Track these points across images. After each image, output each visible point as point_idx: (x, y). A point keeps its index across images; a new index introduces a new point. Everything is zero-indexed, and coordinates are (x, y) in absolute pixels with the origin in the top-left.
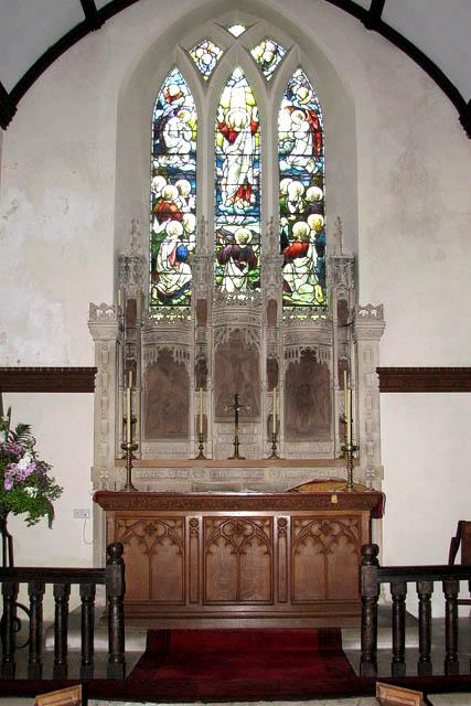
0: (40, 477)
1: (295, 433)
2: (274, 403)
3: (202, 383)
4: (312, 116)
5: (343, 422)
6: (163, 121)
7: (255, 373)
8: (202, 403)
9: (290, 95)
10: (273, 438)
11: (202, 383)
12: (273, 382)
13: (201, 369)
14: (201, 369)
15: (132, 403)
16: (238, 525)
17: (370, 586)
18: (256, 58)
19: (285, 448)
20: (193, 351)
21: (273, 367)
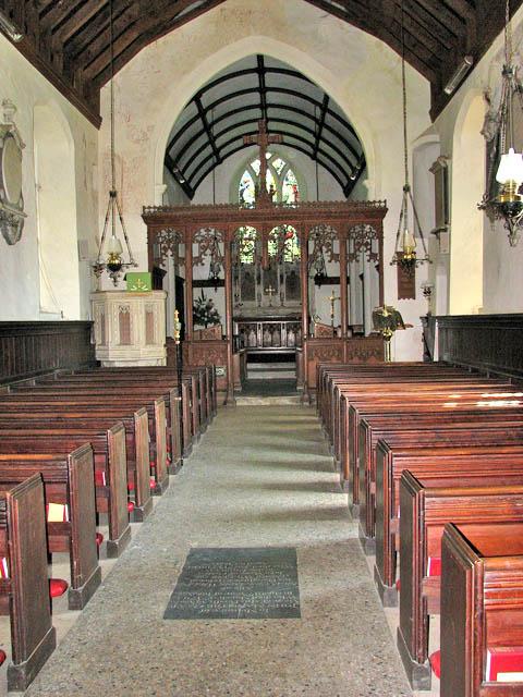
0: (216, 314)
1: (289, 298)
2: (283, 288)
3: (259, 283)
4: (295, 187)
5: (237, 278)
6: (243, 190)
7: (265, 278)
8: (259, 289)
9: (287, 180)
10: (282, 300)
11: (259, 283)
12: (282, 282)
13: (259, 278)
14: (259, 278)
15: (237, 290)
16: (271, 326)
17: (259, 601)
18: (284, 194)
19: (286, 303)
20: (256, 272)
21: (282, 277)
